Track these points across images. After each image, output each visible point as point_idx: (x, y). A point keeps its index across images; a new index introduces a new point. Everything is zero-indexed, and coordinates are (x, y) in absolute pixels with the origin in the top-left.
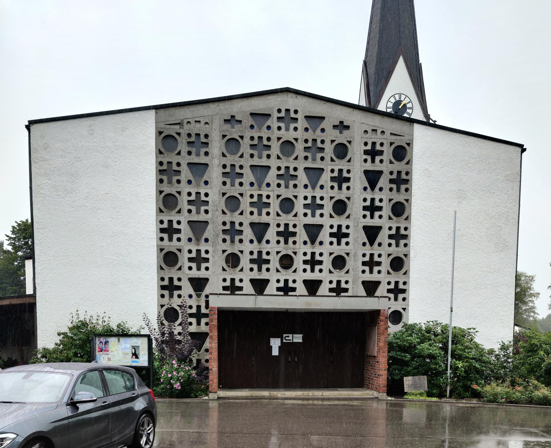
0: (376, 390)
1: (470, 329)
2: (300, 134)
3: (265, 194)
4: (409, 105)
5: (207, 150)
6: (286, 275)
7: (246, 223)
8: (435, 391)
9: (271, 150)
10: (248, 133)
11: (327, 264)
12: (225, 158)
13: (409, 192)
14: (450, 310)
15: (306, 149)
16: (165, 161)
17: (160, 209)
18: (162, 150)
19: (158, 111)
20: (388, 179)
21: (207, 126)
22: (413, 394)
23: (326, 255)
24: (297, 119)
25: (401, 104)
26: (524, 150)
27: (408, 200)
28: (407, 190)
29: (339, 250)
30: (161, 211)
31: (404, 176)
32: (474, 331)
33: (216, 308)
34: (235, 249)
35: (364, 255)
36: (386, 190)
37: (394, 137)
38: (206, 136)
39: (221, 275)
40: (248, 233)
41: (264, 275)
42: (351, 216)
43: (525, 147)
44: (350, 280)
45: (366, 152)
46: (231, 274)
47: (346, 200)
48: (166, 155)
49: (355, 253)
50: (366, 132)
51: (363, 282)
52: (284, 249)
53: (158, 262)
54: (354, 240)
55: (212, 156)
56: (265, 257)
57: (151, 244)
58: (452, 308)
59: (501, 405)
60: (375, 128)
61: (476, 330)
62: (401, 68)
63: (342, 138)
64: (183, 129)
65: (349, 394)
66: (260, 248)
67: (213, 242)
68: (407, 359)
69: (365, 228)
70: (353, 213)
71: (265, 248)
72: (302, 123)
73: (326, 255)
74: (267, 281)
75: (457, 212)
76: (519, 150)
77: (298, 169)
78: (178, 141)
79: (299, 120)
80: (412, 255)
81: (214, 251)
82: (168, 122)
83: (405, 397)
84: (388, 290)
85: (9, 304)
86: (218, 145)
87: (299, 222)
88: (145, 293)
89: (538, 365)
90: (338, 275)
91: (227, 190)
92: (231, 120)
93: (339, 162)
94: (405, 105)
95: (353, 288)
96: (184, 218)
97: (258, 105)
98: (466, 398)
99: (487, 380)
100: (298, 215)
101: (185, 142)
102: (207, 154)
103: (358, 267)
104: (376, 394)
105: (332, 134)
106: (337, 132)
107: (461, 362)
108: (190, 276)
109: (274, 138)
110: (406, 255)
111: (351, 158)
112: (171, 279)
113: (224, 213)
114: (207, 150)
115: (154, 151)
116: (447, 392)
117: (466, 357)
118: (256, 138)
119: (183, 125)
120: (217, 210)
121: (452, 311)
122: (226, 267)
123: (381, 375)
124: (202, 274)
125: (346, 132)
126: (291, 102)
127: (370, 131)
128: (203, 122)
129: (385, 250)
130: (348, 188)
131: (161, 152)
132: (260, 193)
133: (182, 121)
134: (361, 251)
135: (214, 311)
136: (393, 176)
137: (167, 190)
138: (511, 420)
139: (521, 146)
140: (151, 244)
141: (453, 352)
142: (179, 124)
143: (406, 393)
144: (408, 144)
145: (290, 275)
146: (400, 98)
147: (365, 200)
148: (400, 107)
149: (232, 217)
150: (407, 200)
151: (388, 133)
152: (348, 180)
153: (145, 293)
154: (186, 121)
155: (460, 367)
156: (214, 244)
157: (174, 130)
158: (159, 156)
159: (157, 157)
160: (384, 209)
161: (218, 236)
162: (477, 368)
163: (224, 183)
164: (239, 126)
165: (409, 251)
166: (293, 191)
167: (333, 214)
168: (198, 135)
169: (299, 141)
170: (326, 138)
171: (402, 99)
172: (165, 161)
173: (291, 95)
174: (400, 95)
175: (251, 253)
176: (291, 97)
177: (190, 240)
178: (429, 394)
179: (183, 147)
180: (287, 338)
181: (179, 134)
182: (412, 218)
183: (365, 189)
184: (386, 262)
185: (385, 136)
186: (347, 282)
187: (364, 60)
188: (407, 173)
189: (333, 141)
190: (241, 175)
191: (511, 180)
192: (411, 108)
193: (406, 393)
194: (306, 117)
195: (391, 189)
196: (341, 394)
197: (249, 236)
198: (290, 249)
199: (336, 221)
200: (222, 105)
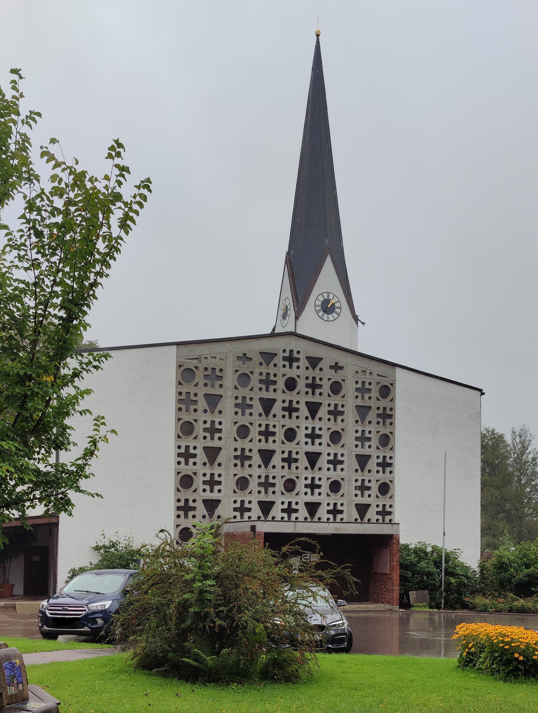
0: (389, 603)
1: (456, 550)
2: (302, 372)
4: (337, 305)
5: (221, 382)
6: (290, 498)
8: (433, 603)
9: (278, 385)
10: (258, 369)
11: (325, 488)
12: (237, 390)
13: (393, 425)
14: (443, 533)
16: (184, 391)
18: (182, 382)
19: (179, 346)
20: (376, 414)
21: (222, 361)
22: (418, 606)
23: (324, 479)
25: (330, 303)
26: (483, 394)
27: (392, 432)
28: (391, 424)
29: (336, 475)
30: (179, 437)
31: (388, 412)
32: (459, 551)
33: (263, 533)
34: (245, 473)
35: (356, 481)
36: (374, 423)
37: (380, 378)
38: (221, 370)
39: (233, 497)
40: (257, 459)
41: (270, 498)
42: (345, 446)
43: (483, 392)
44: (345, 503)
45: (357, 390)
46: (241, 496)
47: (341, 431)
48: (185, 386)
49: (349, 479)
51: (357, 505)
52: (288, 474)
53: (175, 485)
54: (348, 467)
55: (226, 389)
56: (271, 480)
57: (170, 467)
58: (444, 533)
59: (492, 614)
60: (364, 370)
61: (461, 551)
62: (328, 266)
63: (337, 377)
64: (201, 363)
65: (365, 607)
66: (267, 473)
67: (226, 467)
68: (408, 576)
69: (357, 456)
70: (347, 443)
71: (272, 472)
72: (303, 363)
73: (324, 479)
74: (273, 503)
75: (447, 453)
76: (479, 393)
77: (301, 403)
78: (196, 374)
79: (301, 359)
80: (396, 481)
81: (226, 475)
83: (412, 608)
84: (377, 512)
85: (32, 524)
86: (232, 379)
87: (301, 449)
88: (162, 514)
89: (509, 581)
90: (334, 498)
91: (238, 420)
92: (245, 358)
93: (335, 397)
94: (333, 304)
95: (348, 510)
96: (200, 444)
97: (267, 345)
98: (458, 609)
99: (473, 593)
100: (300, 443)
101: (202, 375)
102: (221, 386)
103: (352, 491)
104: (388, 606)
107: (453, 578)
108: (204, 498)
109: (280, 374)
110: (391, 481)
111: (344, 395)
112: (187, 501)
113: (235, 440)
114: (221, 382)
115: (174, 382)
116: (442, 605)
117: (457, 574)
118: (264, 374)
119: (200, 360)
120: (230, 437)
121: (444, 535)
122: (236, 490)
123: (395, 590)
124: (215, 496)
125: (340, 372)
126: (294, 344)
127: (360, 372)
128: (218, 358)
129: (324, 474)
130: (343, 421)
131: (180, 383)
132: (268, 423)
133: (200, 356)
134: (354, 477)
135: (262, 535)
136: (380, 411)
137: (186, 418)
138: (195, 659)
139: (480, 390)
140: (170, 467)
141: (446, 570)
143: (411, 606)
144: (392, 384)
145: (293, 498)
146: (328, 297)
147: (357, 431)
148: (329, 306)
149: (243, 444)
150: (391, 433)
151: (375, 374)
152: (342, 413)
153: (162, 514)
154: (203, 356)
155: (453, 582)
156: (227, 468)
157: (192, 364)
158: (179, 386)
159: (177, 388)
160: (373, 439)
161: (230, 461)
162: (466, 583)
163: (236, 413)
164: (250, 362)
165: (393, 478)
166: (296, 422)
167: (330, 443)
168: (214, 369)
169: (301, 377)
170: (324, 376)
171: (331, 298)
172: (184, 391)
173: (294, 338)
174: (328, 293)
175: (259, 477)
176: (295, 340)
177: (205, 464)
178: (431, 607)
179: (199, 378)
180: (305, 558)
181: (197, 368)
182: (396, 448)
183: (357, 421)
185: (372, 377)
186: (342, 505)
187: (287, 252)
188: (391, 409)
189: (329, 379)
191: (474, 418)
192: (340, 308)
193: (411, 606)
195: (378, 423)
196: (359, 607)
197: (258, 461)
198: (294, 473)
199: (333, 450)
200: (235, 344)
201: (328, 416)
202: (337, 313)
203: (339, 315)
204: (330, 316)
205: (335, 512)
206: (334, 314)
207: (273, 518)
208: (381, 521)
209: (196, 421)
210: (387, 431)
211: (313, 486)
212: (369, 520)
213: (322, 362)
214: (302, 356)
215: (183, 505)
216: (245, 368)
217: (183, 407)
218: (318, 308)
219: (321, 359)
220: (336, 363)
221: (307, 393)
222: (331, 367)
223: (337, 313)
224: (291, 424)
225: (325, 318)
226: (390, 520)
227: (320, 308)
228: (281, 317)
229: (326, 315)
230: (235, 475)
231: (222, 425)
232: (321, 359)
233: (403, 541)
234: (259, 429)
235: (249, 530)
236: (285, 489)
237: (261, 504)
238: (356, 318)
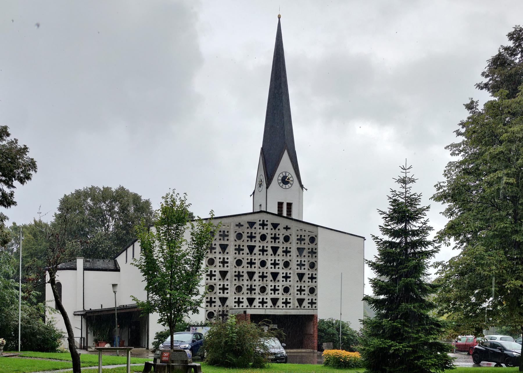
7: (245, 272)
15: (272, 238)
63: (287, 233)
72: (270, 226)
92: (239, 225)
174: (286, 172)
183: (298, 256)
192: (293, 181)
203: (292, 185)
211: (275, 290)
212: (304, 307)
214: (269, 223)
216: (240, 231)
218: (279, 181)
225: (284, 187)
227: (281, 181)
229: (284, 185)
235: (243, 313)
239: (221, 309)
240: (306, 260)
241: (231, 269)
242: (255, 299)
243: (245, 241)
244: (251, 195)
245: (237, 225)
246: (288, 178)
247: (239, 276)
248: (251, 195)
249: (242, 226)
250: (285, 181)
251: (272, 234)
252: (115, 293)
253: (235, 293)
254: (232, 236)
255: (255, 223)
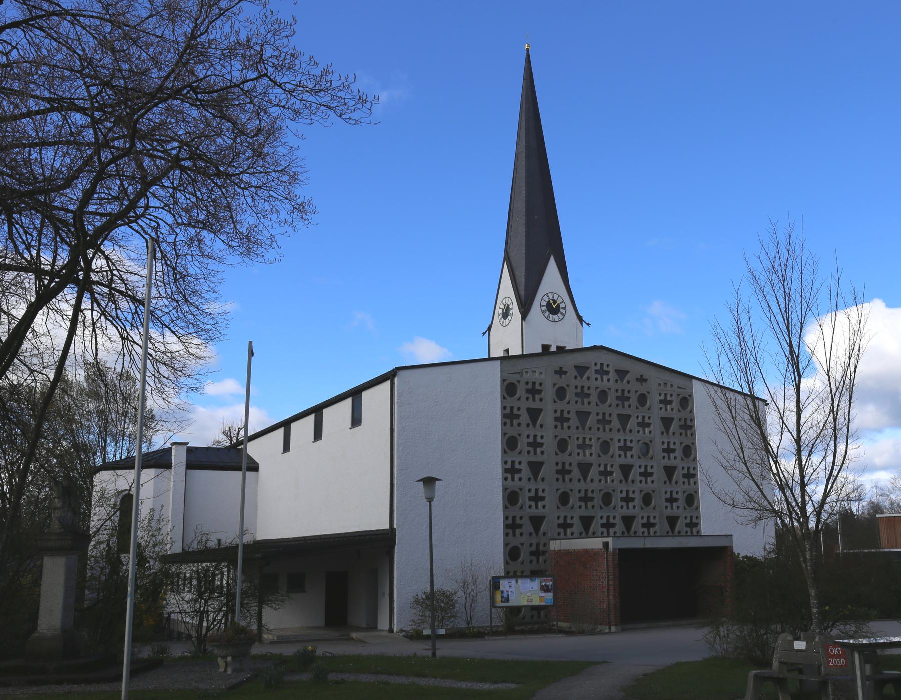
3: (588, 437)
4: (562, 306)
7: (574, 464)
15: (618, 398)
17: (505, 451)
23: (637, 493)
24: (608, 372)
37: (680, 390)
38: (540, 385)
50: (659, 385)
63: (642, 389)
72: (612, 376)
82: (750, 407)
92: (560, 372)
105: (635, 386)
106: (639, 384)
119: (522, 374)
126: (604, 359)
129: (637, 487)
142: (519, 373)
147: (663, 443)
154: (524, 371)
173: (605, 352)
174: (553, 294)
183: (662, 433)
184: (638, 498)
190: (518, 417)
192: (564, 309)
194: (616, 371)
201: (637, 429)
202: (562, 314)
203: (564, 315)
204: (556, 317)
205: (648, 525)
206: (559, 315)
207: (635, 533)
208: (689, 534)
209: (611, 440)
210: (688, 442)
211: (627, 500)
212: (635, 533)
213: (629, 374)
214: (611, 370)
215: (388, 528)
216: (562, 382)
217: (508, 421)
218: (543, 309)
219: (628, 372)
220: (642, 376)
221: (617, 405)
222: (637, 380)
223: (562, 314)
224: (605, 437)
225: (551, 319)
226: (698, 532)
227: (545, 308)
228: (499, 315)
229: (551, 316)
230: (557, 490)
231: (544, 439)
232: (628, 372)
233: (736, 551)
234: (576, 443)
235: (601, 547)
236: (603, 504)
237: (582, 519)
238: (580, 319)
239: (534, 541)
240: (677, 442)
241: (549, 456)
242: (593, 517)
243: (632, 393)
244: (484, 334)
245: (556, 372)
246: (551, 302)
247: (563, 472)
248: (484, 334)
249: (565, 373)
250: (553, 309)
251: (617, 391)
252: (430, 502)
253: (558, 508)
254: (549, 393)
255: (588, 368)
